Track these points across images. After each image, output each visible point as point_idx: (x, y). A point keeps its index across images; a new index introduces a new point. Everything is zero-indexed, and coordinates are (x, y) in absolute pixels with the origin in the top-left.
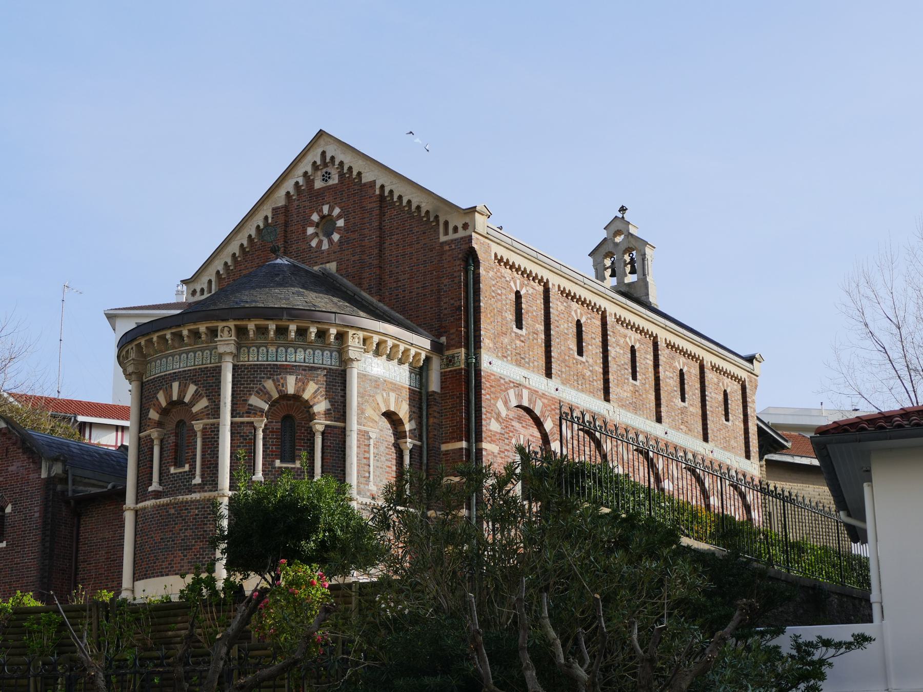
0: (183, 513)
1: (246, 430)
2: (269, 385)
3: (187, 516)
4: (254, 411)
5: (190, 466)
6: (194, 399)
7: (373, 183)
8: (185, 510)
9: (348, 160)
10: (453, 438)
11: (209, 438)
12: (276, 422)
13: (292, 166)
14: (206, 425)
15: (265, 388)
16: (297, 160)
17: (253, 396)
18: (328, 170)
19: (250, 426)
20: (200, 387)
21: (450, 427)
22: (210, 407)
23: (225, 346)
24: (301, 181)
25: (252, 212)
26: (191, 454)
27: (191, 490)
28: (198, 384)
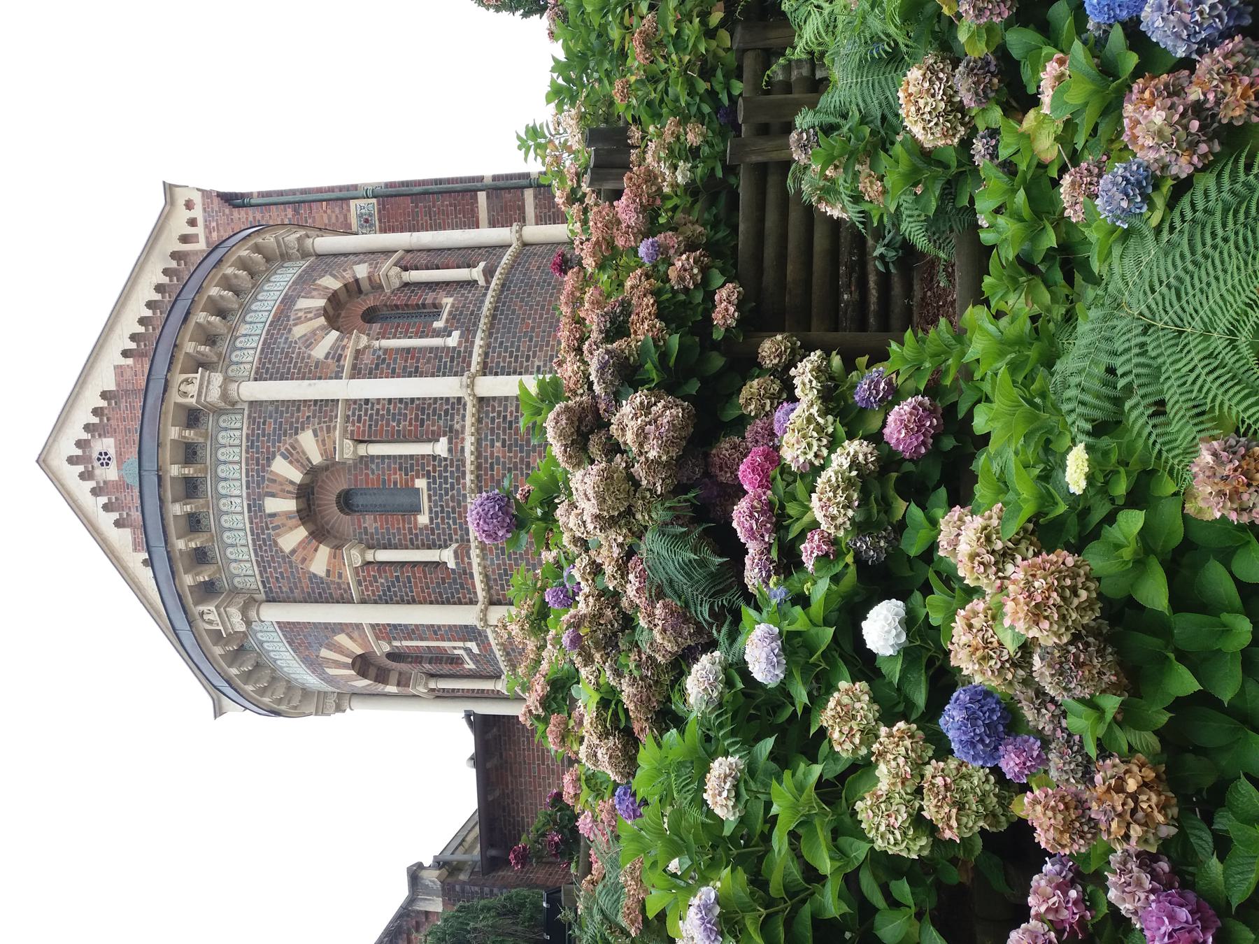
0: (498, 472)
1: (367, 359)
2: (299, 331)
3: (504, 463)
4: (336, 355)
5: (418, 477)
6: (298, 461)
7: (119, 370)
10: (472, 210)
11: (370, 425)
13: (79, 513)
14: (345, 430)
15: (305, 335)
16: (72, 504)
17: (312, 353)
18: (95, 455)
19: (363, 354)
20: (279, 450)
21: (456, 217)
22: (317, 426)
23: (211, 387)
25: (133, 586)
26: (398, 476)
28: (274, 452)
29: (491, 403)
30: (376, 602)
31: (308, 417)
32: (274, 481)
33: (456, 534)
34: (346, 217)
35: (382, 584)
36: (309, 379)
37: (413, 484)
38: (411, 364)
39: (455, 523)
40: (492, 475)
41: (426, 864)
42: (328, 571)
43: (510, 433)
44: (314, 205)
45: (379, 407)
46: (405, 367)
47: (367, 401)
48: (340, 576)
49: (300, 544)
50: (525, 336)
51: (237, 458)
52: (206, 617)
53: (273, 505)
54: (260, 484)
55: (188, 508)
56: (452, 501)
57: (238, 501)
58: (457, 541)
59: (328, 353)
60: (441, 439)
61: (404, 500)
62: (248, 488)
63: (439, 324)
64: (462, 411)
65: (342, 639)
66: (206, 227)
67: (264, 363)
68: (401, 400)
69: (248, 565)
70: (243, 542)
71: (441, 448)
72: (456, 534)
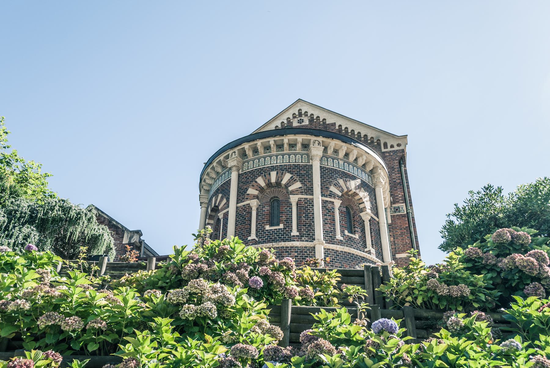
1: (330, 206)
2: (341, 182)
4: (332, 195)
5: (284, 225)
6: (290, 182)
7: (334, 124)
8: (286, 252)
9: (316, 113)
12: (343, 207)
22: (303, 188)
24: (285, 122)
27: (290, 239)
29: (313, 251)
30: (237, 212)
31: (307, 185)
32: (282, 174)
33: (262, 240)
34: (398, 202)
35: (243, 214)
36: (321, 185)
37: (281, 223)
38: (328, 222)
39: (266, 239)
40: (284, 252)
41: (141, 237)
42: (249, 194)
43: (300, 259)
44: (402, 190)
45: (311, 210)
46: (327, 219)
47: (313, 206)
48: (247, 199)
49: (259, 184)
50: (342, 265)
51: (291, 161)
52: (234, 154)
53: (273, 175)
54: (281, 170)
55: (272, 146)
56: (274, 238)
57: (275, 162)
58: (259, 240)
59: (332, 192)
60: (298, 233)
61: (275, 221)
62: (280, 165)
63: (346, 232)
64: (309, 240)
65: (225, 201)
66: (391, 151)
67: (327, 170)
68: (313, 218)
69: (252, 167)
70: (260, 165)
71: (295, 233)
72: (262, 240)
